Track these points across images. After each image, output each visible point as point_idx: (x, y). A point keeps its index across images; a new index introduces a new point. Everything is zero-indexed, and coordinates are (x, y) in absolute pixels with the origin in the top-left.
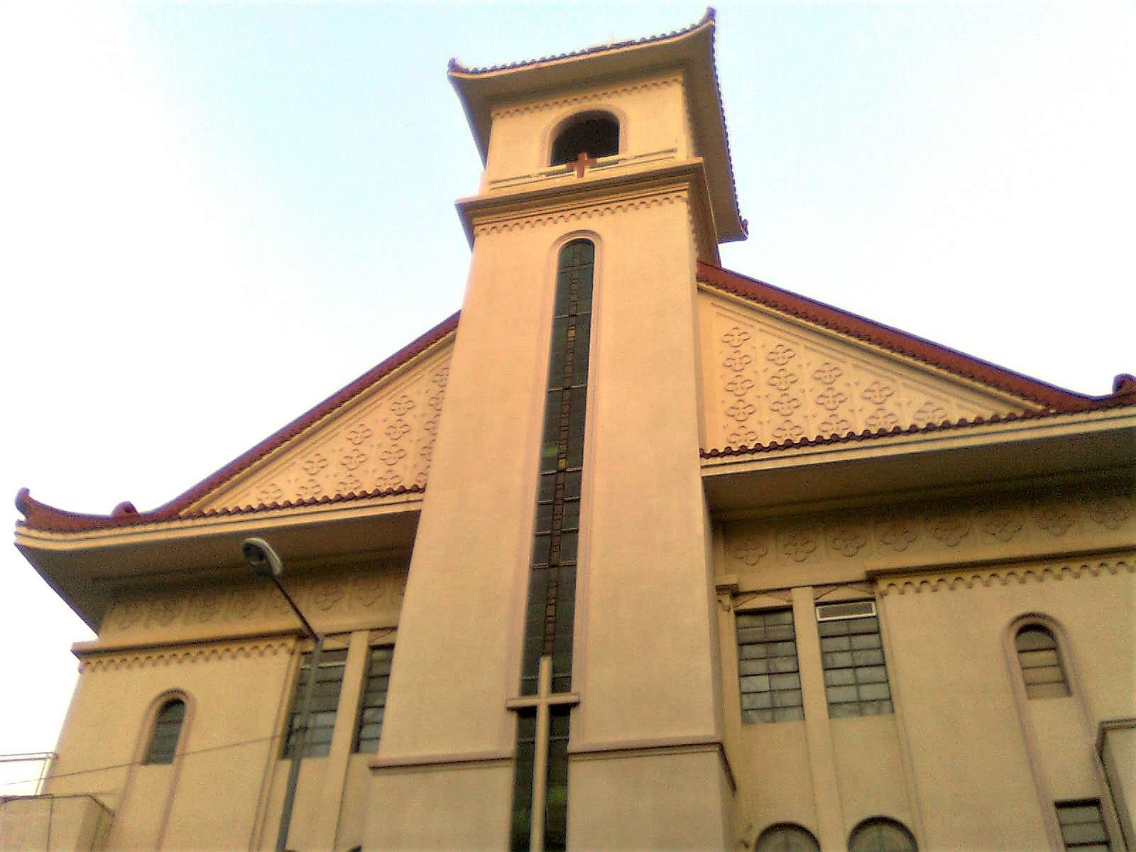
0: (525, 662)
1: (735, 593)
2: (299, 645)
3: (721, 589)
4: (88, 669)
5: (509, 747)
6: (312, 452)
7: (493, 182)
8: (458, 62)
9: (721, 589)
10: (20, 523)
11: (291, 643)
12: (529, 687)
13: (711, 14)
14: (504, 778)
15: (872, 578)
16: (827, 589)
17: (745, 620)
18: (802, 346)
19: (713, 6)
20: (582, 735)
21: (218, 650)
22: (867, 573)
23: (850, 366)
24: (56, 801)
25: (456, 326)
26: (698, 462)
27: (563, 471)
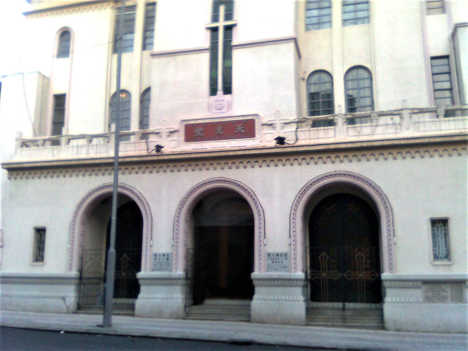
5: (207, 44)
12: (215, 18)
14: (206, 57)
20: (237, 38)
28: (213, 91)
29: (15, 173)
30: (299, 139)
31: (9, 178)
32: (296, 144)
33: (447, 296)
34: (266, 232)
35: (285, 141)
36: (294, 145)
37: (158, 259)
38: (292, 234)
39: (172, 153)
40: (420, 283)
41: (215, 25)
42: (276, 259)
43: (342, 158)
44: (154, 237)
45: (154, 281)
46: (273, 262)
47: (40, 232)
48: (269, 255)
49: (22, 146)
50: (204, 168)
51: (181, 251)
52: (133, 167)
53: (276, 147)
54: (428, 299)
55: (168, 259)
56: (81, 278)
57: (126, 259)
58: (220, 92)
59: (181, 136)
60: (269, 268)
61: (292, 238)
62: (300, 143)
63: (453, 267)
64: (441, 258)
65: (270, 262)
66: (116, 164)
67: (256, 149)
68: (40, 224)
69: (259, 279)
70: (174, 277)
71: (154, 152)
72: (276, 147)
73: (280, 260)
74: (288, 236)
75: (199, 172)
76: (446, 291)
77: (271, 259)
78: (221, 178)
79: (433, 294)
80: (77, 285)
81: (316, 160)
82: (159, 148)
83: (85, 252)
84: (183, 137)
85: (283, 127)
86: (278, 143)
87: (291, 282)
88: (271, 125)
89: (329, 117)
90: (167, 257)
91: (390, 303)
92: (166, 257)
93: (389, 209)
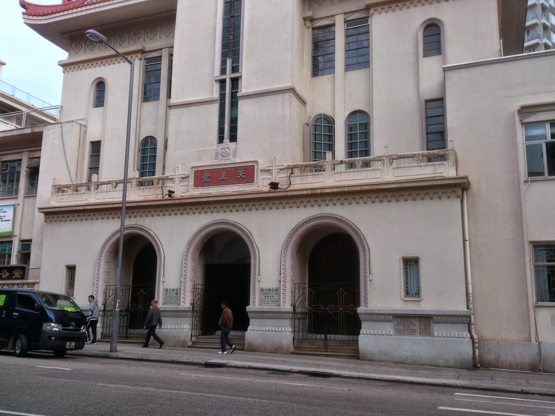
0: (222, 364)
1: (312, 20)
3: (305, 19)
5: (216, 95)
11: (139, 56)
14: (216, 107)
16: (350, 14)
17: (316, 32)
20: (244, 88)
21: (392, 6)
22: (366, 5)
24: (62, 124)
28: (221, 140)
29: (50, 217)
30: (292, 183)
31: (46, 222)
32: (289, 189)
33: (416, 330)
34: (260, 270)
35: (279, 186)
36: (286, 190)
37: (168, 294)
38: (282, 271)
40: (391, 317)
41: (223, 77)
42: (268, 294)
43: (142, 213)
44: (165, 275)
45: (263, 315)
46: (266, 297)
47: (71, 269)
48: (262, 290)
49: (58, 192)
51: (189, 286)
52: (73, 215)
54: (398, 332)
55: (177, 294)
56: (294, 312)
57: (343, 293)
58: (226, 140)
60: (261, 302)
61: (282, 275)
62: (293, 187)
64: (412, 294)
66: (124, 209)
68: (71, 263)
71: (167, 197)
72: (269, 192)
73: (272, 295)
74: (279, 273)
75: (107, 220)
76: (415, 325)
78: (224, 221)
79: (403, 327)
81: (320, 203)
82: (171, 192)
86: (271, 188)
87: (283, 315)
89: (441, 152)
90: (178, 291)
92: (175, 292)
93: (367, 249)
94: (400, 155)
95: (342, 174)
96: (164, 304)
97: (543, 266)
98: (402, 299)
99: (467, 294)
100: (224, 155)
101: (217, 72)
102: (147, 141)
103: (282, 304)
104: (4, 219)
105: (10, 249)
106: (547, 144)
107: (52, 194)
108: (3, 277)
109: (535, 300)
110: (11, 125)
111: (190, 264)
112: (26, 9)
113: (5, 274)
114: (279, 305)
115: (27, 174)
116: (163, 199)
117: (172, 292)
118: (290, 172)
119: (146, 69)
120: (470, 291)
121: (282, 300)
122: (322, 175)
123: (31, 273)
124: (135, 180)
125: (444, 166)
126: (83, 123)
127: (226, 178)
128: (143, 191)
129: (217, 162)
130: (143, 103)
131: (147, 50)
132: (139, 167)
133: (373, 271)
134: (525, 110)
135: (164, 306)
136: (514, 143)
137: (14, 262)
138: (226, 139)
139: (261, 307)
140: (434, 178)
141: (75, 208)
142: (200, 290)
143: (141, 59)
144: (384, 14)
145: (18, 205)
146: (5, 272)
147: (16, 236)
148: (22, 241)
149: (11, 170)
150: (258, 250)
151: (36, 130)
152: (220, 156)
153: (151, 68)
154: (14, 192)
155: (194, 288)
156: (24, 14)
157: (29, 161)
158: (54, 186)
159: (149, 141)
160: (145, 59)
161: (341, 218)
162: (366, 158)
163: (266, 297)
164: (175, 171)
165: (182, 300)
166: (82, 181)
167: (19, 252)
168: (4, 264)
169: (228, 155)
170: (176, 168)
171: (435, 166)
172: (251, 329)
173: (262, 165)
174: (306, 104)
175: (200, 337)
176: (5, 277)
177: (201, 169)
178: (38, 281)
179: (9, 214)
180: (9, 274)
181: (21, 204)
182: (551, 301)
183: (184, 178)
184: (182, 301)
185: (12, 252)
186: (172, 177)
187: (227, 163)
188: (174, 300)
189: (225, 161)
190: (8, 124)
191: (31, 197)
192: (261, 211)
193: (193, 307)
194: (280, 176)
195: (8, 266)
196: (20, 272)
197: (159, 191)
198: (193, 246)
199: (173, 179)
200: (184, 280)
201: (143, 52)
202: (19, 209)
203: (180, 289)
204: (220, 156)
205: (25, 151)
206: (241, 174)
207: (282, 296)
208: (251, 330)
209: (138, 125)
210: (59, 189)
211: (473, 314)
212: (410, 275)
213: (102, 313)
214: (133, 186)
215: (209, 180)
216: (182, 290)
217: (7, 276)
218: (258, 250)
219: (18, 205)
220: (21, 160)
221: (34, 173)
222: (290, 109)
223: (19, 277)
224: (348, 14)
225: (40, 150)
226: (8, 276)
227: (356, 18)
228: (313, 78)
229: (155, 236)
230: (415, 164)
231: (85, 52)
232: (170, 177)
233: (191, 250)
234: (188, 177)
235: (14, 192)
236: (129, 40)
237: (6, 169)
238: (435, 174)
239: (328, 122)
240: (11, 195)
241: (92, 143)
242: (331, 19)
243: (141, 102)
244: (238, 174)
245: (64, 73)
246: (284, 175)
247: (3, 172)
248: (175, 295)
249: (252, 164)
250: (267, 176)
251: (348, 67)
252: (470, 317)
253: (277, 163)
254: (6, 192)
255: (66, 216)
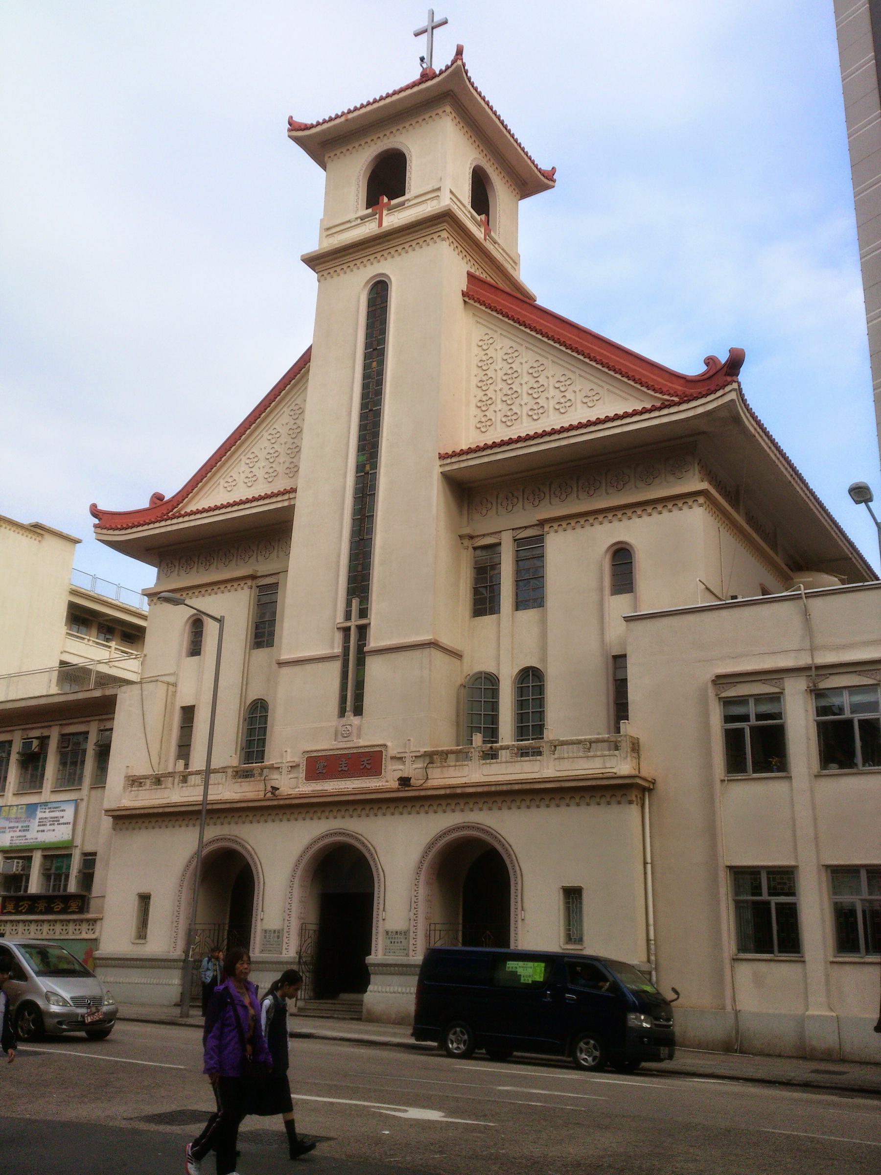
2: (254, 582)
3: (461, 537)
4: (152, 604)
5: (338, 650)
6: (248, 451)
7: (328, 229)
8: (296, 119)
9: (461, 537)
10: (96, 526)
11: (249, 582)
12: (348, 616)
13: (460, 52)
14: (337, 666)
15: (542, 523)
16: (521, 530)
17: (479, 552)
18: (524, 346)
19: (461, 43)
20: (374, 642)
23: (550, 362)
25: (310, 362)
26: (438, 462)
27: (368, 473)
28: (342, 713)
30: (429, 777)
31: (114, 829)
35: (412, 782)
36: (421, 788)
39: (118, 809)
41: (348, 624)
42: (395, 938)
44: (264, 909)
46: (391, 942)
47: (145, 899)
48: (387, 933)
49: (132, 785)
50: (485, 807)
53: (398, 790)
55: (278, 937)
59: (302, 773)
62: (432, 783)
63: (146, 945)
65: (388, 941)
66: (204, 813)
67: (241, 802)
68: (144, 890)
69: (374, 965)
70: (282, 960)
71: (269, 795)
72: (398, 790)
77: (389, 938)
80: (183, 968)
83: (433, 927)
84: (302, 775)
85: (290, 772)
86: (400, 784)
88: (401, 758)
90: (278, 934)
91: (371, 991)
92: (276, 934)
94: (563, 741)
95: (492, 765)
96: (262, 951)
97: (747, 902)
98: (561, 947)
99: (648, 940)
100: (345, 735)
101: (340, 618)
102: (257, 705)
103: (411, 953)
104: (62, 821)
105: (69, 867)
106: (752, 728)
107: (124, 788)
108: (55, 910)
109: (733, 948)
110: (89, 640)
111: (297, 893)
112: (100, 519)
113: (58, 906)
114: (407, 955)
115: (96, 754)
116: (264, 799)
117: (272, 935)
118: (427, 760)
119: (259, 600)
120: (652, 937)
121: (411, 947)
122: (467, 767)
123: (93, 903)
124: (232, 770)
125: (616, 758)
126: (171, 679)
127: (346, 769)
128: (241, 786)
129: (336, 744)
130: (252, 651)
131: (259, 574)
132: (244, 745)
133: (526, 905)
134: (721, 681)
135: (262, 955)
136: (707, 724)
137: (72, 887)
138: (349, 711)
139: (385, 957)
140: (601, 775)
141: (151, 811)
142: (311, 932)
143: (251, 588)
144: (561, 534)
145: (82, 800)
146: (58, 903)
147: (77, 846)
148: (85, 854)
149: (74, 748)
150: (384, 875)
151: (108, 692)
152: (340, 736)
153: (265, 599)
154: (77, 779)
155: (303, 930)
156: (96, 526)
157: (98, 735)
158: (128, 777)
159: (259, 705)
160: (258, 587)
161: (488, 829)
162: (521, 744)
163: (391, 942)
164: (282, 756)
165: (285, 946)
166: (120, 804)
167: (80, 872)
168: (59, 891)
169: (350, 735)
170: (284, 753)
171: (605, 758)
172: (372, 989)
173: (393, 750)
174: (461, 656)
175: (310, 1001)
176: (58, 910)
177: (315, 754)
178: (100, 916)
179: (68, 814)
180: (63, 906)
181: (85, 798)
182: (757, 952)
183: (294, 767)
184: (284, 948)
185: (71, 872)
186: (278, 766)
187: (348, 746)
188: (275, 946)
189: (346, 744)
190: (84, 639)
191: (100, 789)
192: (389, 818)
193: (300, 958)
194: (414, 766)
195: (64, 894)
196: (77, 903)
197: (261, 786)
198: (301, 866)
199: (279, 768)
200: (287, 918)
201: (253, 577)
202: (83, 806)
203: (283, 930)
204: (340, 736)
205: (95, 720)
206: (366, 762)
207: (412, 942)
208: (371, 991)
209: (245, 683)
210: (135, 782)
211: (656, 969)
212: (573, 912)
213: (182, 963)
214: (228, 777)
215: (324, 771)
216: (285, 931)
217: (60, 907)
218: (384, 875)
219: (82, 800)
220: (87, 733)
221: (104, 752)
222: (430, 670)
223: (77, 910)
224: (517, 531)
225: (113, 719)
226: (62, 908)
227: (526, 536)
228: (473, 619)
229: (253, 853)
230: (581, 754)
231: (178, 575)
232: (275, 766)
233: (299, 873)
234: (298, 766)
235: (77, 779)
236: (237, 561)
237: (67, 745)
238: (604, 770)
239: (491, 682)
240: (73, 785)
241: (184, 708)
242: (496, 536)
243: (250, 649)
244: (362, 763)
245: (149, 605)
246: (419, 765)
247: (63, 750)
248: (276, 939)
249: (380, 749)
250: (398, 766)
251: (520, 604)
252: (650, 973)
253: (412, 747)
254: (66, 781)
255: (140, 821)
